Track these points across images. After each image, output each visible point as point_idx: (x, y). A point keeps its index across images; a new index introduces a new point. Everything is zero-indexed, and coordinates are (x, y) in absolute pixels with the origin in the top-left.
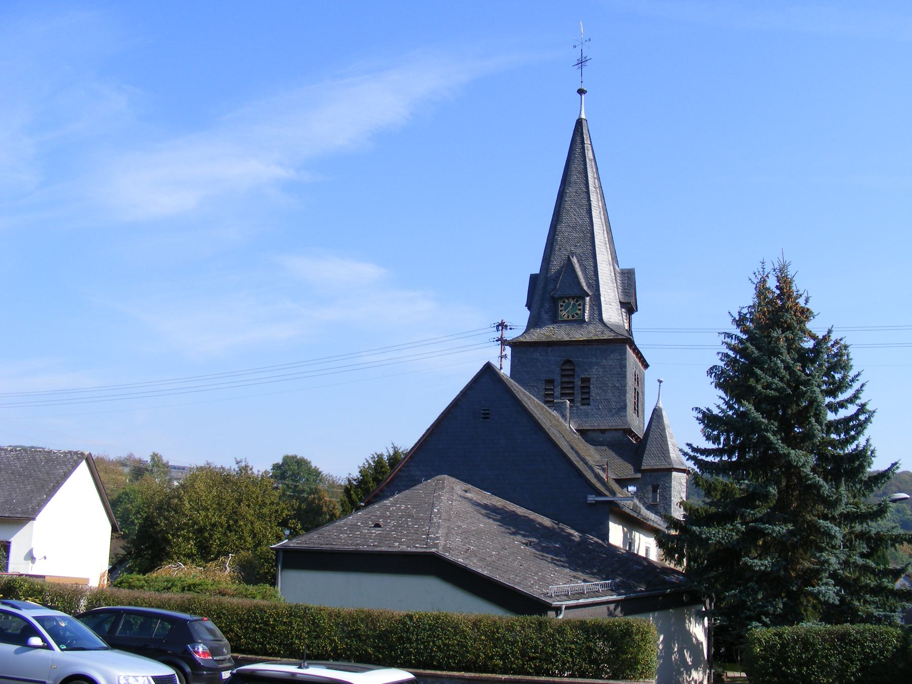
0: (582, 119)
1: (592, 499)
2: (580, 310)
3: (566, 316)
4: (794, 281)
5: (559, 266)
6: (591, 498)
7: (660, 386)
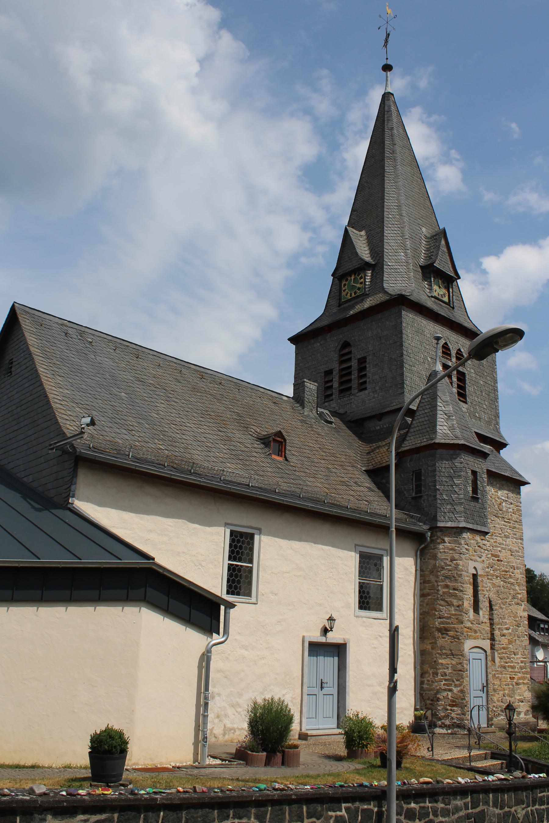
2: (361, 283)
3: (349, 294)
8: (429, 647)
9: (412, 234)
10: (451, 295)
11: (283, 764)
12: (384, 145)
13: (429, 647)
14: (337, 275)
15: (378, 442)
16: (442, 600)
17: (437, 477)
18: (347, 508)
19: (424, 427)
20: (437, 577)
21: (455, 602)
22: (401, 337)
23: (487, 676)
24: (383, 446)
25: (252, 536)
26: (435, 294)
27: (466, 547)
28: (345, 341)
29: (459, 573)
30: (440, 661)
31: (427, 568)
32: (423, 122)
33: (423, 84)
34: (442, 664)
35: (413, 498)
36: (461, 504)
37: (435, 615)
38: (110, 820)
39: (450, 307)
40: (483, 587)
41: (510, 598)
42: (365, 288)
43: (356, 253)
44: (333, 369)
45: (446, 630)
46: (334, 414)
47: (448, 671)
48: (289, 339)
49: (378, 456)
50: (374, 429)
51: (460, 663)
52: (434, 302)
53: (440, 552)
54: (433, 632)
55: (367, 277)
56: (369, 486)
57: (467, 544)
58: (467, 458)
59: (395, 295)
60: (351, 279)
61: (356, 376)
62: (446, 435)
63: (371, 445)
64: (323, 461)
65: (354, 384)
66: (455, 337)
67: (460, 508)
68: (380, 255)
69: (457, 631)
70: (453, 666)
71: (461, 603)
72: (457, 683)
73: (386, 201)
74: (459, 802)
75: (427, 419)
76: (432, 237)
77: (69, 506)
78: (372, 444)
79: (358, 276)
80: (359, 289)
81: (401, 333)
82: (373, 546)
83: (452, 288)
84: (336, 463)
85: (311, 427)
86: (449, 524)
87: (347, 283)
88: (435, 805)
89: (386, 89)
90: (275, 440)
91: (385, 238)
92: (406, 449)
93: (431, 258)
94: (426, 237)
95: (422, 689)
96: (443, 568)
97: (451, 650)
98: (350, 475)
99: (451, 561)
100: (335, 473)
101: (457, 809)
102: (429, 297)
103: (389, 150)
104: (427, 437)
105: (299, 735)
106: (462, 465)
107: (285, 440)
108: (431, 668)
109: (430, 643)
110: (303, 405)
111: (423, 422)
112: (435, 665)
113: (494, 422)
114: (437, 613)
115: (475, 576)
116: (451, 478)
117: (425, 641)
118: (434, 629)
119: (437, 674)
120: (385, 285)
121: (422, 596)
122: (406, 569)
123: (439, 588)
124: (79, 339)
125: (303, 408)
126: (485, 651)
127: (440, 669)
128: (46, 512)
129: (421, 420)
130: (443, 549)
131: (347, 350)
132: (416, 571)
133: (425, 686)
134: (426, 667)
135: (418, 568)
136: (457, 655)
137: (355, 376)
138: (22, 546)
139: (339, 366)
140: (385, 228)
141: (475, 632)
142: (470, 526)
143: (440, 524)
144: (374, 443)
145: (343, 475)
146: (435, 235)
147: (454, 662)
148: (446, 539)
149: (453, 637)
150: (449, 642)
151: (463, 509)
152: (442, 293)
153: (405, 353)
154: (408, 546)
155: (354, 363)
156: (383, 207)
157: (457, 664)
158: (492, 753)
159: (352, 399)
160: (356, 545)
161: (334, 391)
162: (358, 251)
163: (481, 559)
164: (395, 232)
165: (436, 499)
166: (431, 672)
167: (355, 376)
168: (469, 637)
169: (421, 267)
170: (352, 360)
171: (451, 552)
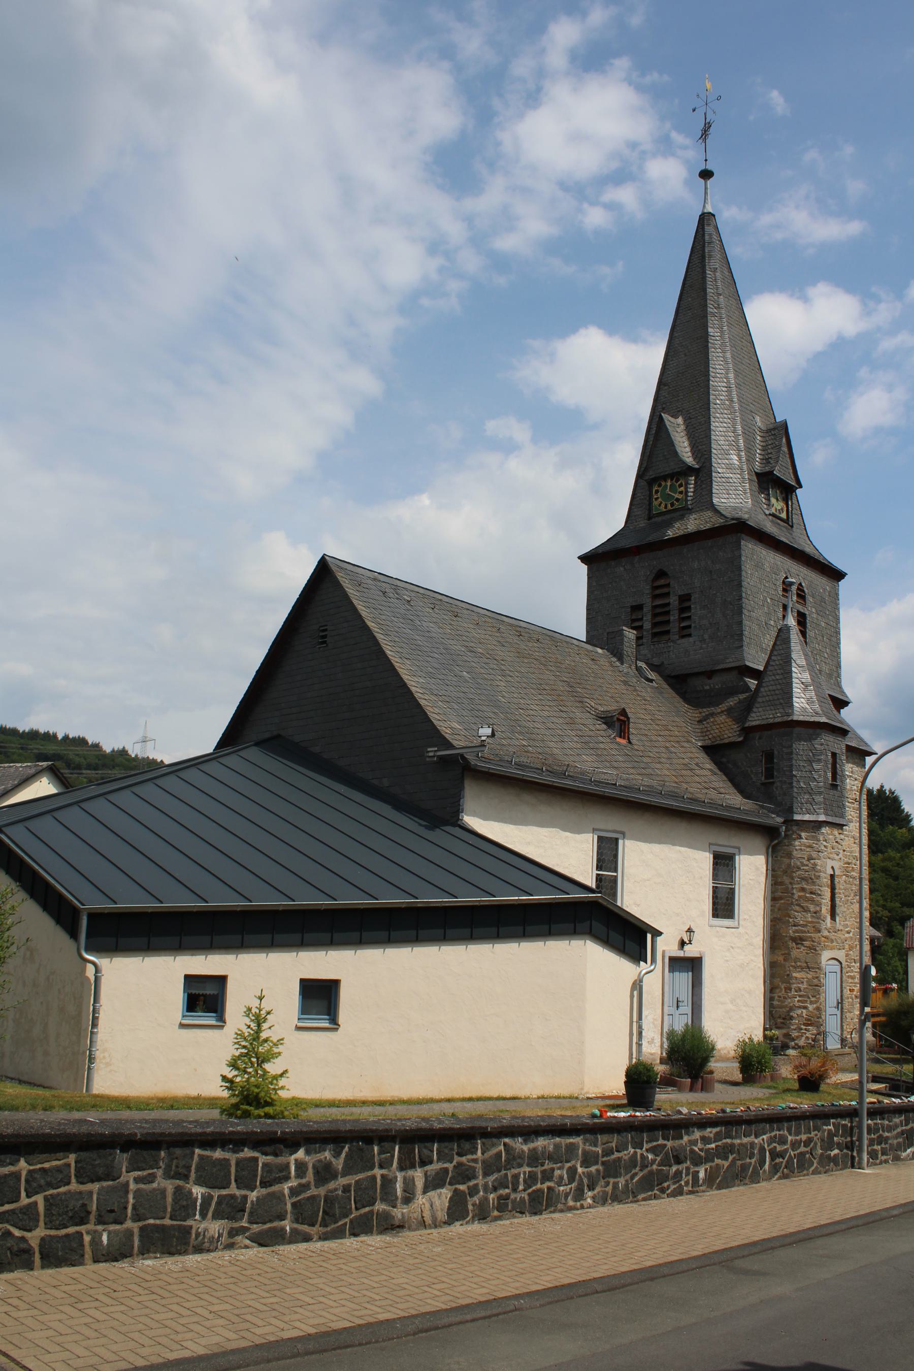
2: (681, 493)
3: (663, 505)
6: (432, 751)
8: (781, 958)
9: (745, 427)
10: (790, 509)
11: (702, 1090)
12: (706, 294)
13: (781, 958)
14: (647, 478)
15: (709, 707)
16: (797, 905)
17: (794, 761)
18: (704, 802)
19: (776, 698)
20: (792, 878)
21: (812, 908)
22: (740, 575)
23: (842, 991)
24: (719, 713)
25: (617, 840)
26: (773, 510)
27: (825, 843)
28: (661, 570)
29: (817, 874)
30: (794, 975)
31: (779, 868)
32: (630, 84)
33: (636, 21)
34: (796, 978)
35: (763, 784)
36: (820, 793)
37: (789, 922)
38: (721, 1131)
39: (788, 524)
40: (840, 889)
41: (852, 895)
42: (686, 501)
43: (676, 453)
45: (802, 939)
46: (653, 667)
47: (802, 986)
48: (579, 558)
49: (714, 727)
51: (817, 977)
52: (772, 521)
53: (796, 850)
54: (786, 942)
55: (689, 486)
56: (710, 767)
57: (825, 841)
58: (827, 738)
59: (733, 519)
60: (666, 486)
61: (677, 617)
62: (805, 709)
63: (701, 710)
64: (660, 739)
65: (674, 627)
66: (796, 568)
67: (819, 799)
68: (706, 456)
69: (813, 941)
70: (809, 980)
71: (818, 909)
72: (813, 999)
73: (711, 378)
74: (897, 1120)
75: (779, 687)
76: (769, 431)
77: (459, 823)
78: (702, 708)
79: (677, 481)
80: (677, 500)
81: (740, 569)
82: (726, 843)
83: (792, 499)
84: (671, 739)
85: (635, 690)
86: (807, 817)
87: (660, 489)
88: (882, 1121)
89: (704, 206)
90: (618, 719)
91: (712, 432)
92: (754, 723)
93: (769, 462)
94: (761, 430)
95: (771, 1006)
96: (799, 868)
97: (807, 963)
98: (689, 755)
99: (809, 860)
100: (675, 753)
101: (896, 1126)
102: (766, 515)
103: (712, 303)
104: (781, 710)
105: (661, 1059)
106: (822, 747)
107: (628, 718)
108: (783, 983)
109: (782, 954)
110: (621, 659)
111: (774, 690)
112: (787, 979)
113: (835, 674)
114: (791, 920)
115: (832, 877)
116: (810, 762)
117: (776, 951)
118: (787, 939)
119: (790, 989)
120: (715, 501)
121: (774, 899)
122: (757, 869)
123: (795, 891)
124: (398, 599)
125: (622, 664)
126: (841, 963)
127: (794, 983)
128: (437, 829)
129: (771, 688)
130: (799, 846)
132: (767, 870)
133: (775, 1003)
134: (777, 981)
135: (770, 867)
136: (813, 968)
137: (674, 617)
138: (145, 803)
139: (652, 603)
140: (712, 419)
141: (832, 941)
142: (830, 819)
143: (797, 817)
144: (705, 708)
145: (682, 755)
146: (774, 429)
147: (809, 976)
148: (803, 834)
149: (809, 947)
150: (804, 954)
151: (822, 800)
152: (780, 508)
153: (744, 595)
154: (759, 842)
155: (674, 600)
156: (709, 388)
157: (813, 978)
158: (873, 1077)
159: (670, 647)
160: (710, 844)
161: (645, 633)
162: (679, 449)
163: (839, 857)
164: (725, 425)
165: (792, 787)
166: (783, 987)
167: (674, 617)
168: (825, 948)
169: (757, 474)
170: (671, 596)
171: (808, 849)
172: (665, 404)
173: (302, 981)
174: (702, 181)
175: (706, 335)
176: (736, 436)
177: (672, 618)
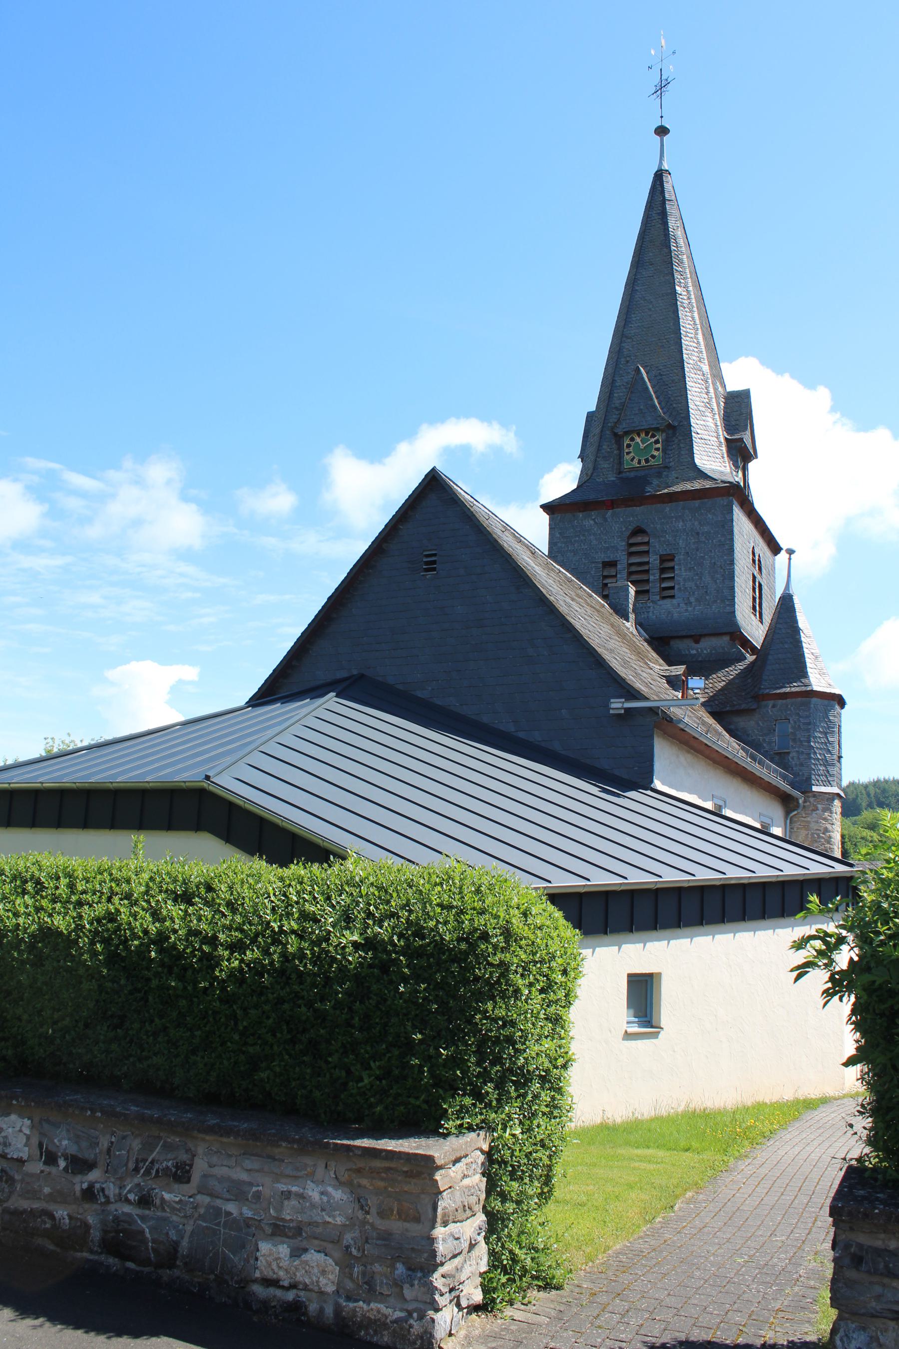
0: (662, 170)
1: (619, 705)
3: (636, 461)
4: (814, 969)
5: (626, 388)
6: (617, 705)
7: (790, 559)
44: (616, 561)
50: (687, 653)
87: (632, 443)
89: (661, 163)
131: (640, 538)
137: (654, 576)
143: (815, 789)
155: (654, 560)
159: (649, 607)
164: (699, 386)
172: (629, 357)
173: (629, 976)
174: (658, 138)
175: (674, 292)
176: (710, 399)
177: (652, 578)
